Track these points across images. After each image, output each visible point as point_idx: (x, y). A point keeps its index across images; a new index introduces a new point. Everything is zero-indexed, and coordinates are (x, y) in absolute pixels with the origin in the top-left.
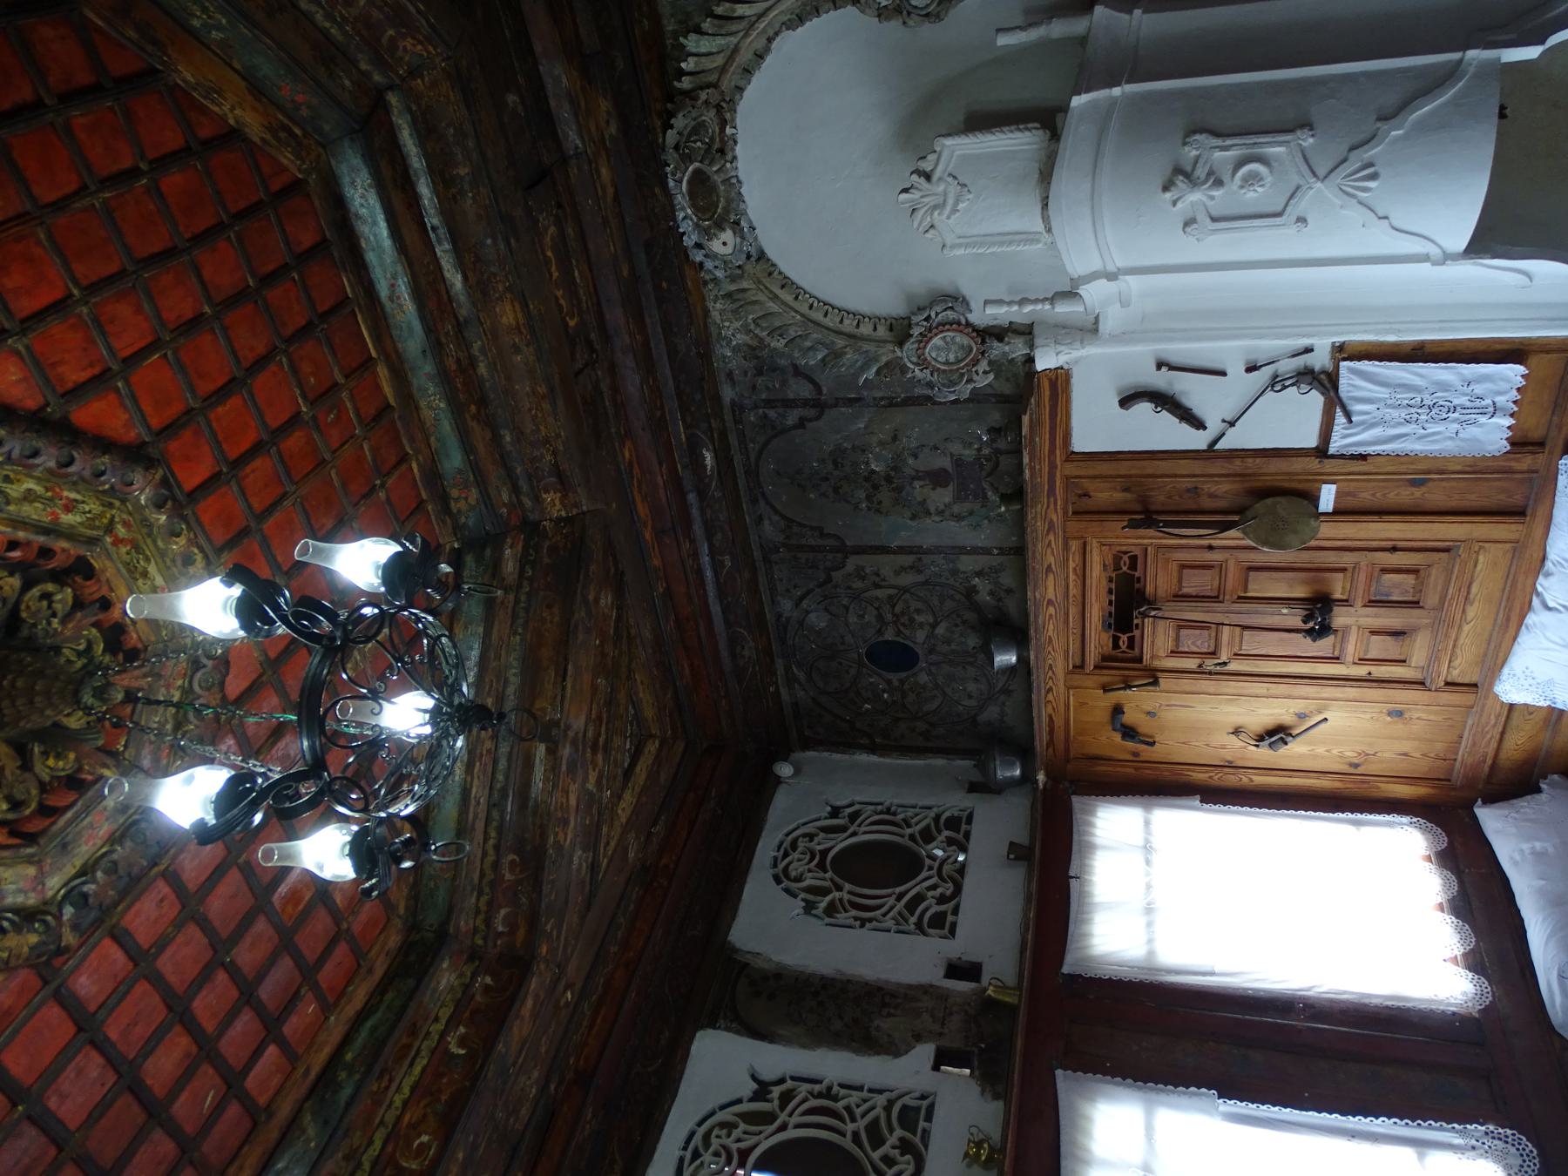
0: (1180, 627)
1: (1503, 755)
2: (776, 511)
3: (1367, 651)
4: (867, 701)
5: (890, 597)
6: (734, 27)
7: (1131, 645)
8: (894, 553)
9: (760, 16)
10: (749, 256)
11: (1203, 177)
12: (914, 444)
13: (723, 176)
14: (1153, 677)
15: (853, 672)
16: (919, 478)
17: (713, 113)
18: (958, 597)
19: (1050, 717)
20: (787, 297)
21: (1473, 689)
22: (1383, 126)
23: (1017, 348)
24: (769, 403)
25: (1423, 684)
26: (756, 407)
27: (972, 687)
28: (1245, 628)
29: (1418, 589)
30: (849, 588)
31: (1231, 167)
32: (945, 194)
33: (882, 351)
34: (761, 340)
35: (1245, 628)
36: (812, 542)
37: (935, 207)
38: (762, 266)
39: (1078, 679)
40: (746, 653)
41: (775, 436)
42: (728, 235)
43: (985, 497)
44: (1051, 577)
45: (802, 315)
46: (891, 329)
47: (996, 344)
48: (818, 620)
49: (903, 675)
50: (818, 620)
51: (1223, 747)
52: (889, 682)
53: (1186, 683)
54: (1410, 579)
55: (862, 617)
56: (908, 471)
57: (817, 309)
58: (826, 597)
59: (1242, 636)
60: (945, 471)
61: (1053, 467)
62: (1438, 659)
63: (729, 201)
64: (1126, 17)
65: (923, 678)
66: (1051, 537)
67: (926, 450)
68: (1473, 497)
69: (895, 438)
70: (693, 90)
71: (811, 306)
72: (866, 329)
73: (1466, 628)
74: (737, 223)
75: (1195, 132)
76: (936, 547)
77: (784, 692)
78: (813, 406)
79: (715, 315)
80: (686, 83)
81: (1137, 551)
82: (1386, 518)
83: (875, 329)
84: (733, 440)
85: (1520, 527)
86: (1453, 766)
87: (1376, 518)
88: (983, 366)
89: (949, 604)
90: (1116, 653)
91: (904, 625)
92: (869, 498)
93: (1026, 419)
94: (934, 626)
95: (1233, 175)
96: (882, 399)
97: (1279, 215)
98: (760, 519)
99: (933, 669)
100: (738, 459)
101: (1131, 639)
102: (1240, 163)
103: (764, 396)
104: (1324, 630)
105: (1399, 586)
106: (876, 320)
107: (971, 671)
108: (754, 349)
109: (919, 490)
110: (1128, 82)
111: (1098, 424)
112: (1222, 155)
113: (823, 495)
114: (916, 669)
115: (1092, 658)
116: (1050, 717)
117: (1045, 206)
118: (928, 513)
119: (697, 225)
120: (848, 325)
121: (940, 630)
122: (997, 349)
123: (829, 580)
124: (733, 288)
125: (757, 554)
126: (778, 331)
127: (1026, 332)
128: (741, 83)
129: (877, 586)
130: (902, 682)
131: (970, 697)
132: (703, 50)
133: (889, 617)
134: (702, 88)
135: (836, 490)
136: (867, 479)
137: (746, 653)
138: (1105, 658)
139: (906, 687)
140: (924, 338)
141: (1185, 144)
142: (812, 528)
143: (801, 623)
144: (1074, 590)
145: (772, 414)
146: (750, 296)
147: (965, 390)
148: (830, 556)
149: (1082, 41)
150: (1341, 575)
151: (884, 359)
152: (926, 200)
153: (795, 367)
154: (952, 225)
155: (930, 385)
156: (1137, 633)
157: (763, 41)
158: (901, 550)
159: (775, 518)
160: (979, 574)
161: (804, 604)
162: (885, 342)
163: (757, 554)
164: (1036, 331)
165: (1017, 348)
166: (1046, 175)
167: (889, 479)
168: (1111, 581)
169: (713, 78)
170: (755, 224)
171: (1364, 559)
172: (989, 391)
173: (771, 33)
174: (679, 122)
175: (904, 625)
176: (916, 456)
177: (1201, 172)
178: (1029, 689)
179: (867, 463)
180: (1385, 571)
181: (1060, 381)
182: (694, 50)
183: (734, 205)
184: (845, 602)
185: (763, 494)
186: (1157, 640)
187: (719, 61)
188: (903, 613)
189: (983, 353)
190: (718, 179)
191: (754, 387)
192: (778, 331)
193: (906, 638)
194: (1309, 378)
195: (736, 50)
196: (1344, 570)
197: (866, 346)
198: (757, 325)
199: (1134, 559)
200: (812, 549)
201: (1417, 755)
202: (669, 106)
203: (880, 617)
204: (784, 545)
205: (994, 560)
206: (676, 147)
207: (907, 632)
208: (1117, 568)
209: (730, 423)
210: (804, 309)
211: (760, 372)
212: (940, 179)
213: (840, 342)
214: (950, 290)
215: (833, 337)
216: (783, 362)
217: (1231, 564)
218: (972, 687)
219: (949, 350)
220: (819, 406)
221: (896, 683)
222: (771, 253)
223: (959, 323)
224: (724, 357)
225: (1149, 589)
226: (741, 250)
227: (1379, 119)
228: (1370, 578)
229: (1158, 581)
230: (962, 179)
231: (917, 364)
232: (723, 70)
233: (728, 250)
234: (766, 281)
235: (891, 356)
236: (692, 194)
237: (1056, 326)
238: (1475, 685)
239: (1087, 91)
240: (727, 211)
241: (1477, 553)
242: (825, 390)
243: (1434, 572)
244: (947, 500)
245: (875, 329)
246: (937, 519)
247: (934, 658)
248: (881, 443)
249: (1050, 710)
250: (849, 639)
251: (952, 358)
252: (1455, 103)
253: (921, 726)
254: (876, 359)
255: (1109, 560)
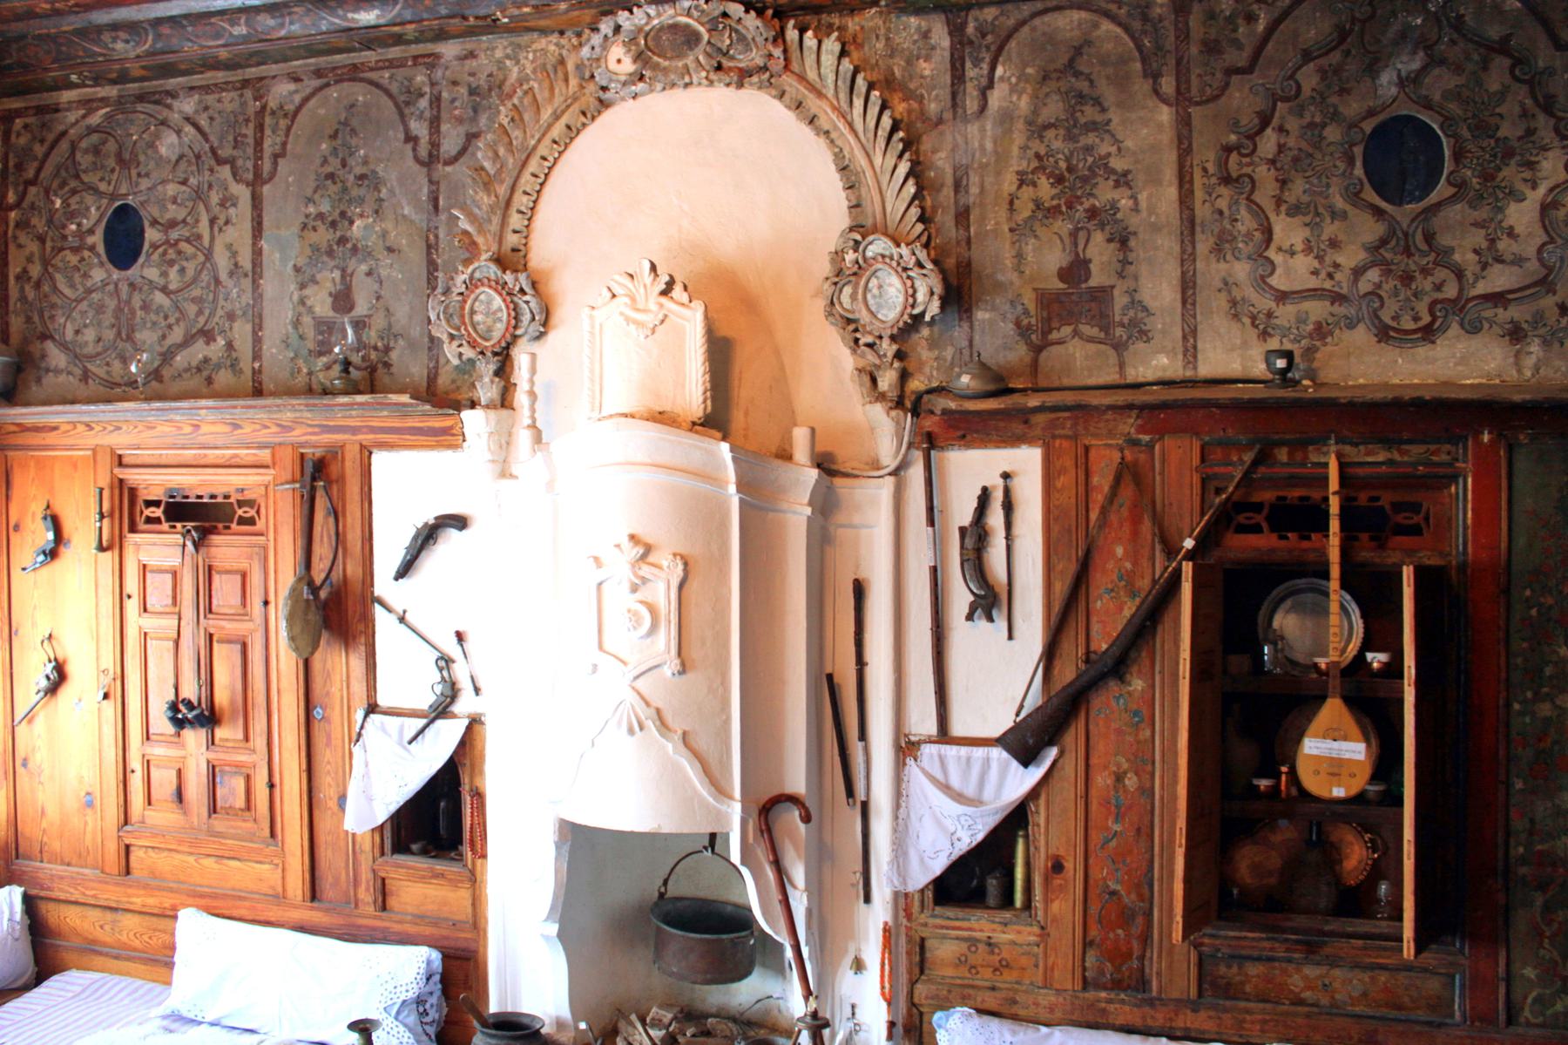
0: (175, 574)
1: (51, 906)
2: (306, 100)
3: (158, 766)
4: (66, 203)
5: (199, 237)
6: (843, 96)
7: (149, 520)
8: (254, 244)
9: (851, 125)
10: (604, 89)
11: (641, 573)
12: (384, 273)
13: (692, 66)
14: (110, 545)
15: (103, 187)
16: (343, 277)
17: (760, 62)
18: (202, 320)
19: (55, 428)
20: (557, 130)
21: (123, 870)
22: (677, 737)
23: (487, 390)
24: (436, 101)
25: (126, 823)
26: (433, 84)
27: (89, 335)
28: (177, 643)
29: (230, 811)
30: (210, 186)
31: (649, 600)
32: (645, 311)
33: (490, 238)
34: (510, 96)
35: (177, 643)
36: (267, 143)
37: (633, 299)
38: (593, 103)
39: (105, 461)
40: (120, 46)
41: (397, 105)
42: (628, 66)
43: (321, 354)
44: (227, 429)
45: (535, 148)
46: (515, 250)
47: (492, 367)
48: (168, 145)
49: (101, 249)
50: (168, 145)
51: (34, 624)
52: (91, 231)
53: (108, 581)
54: (240, 802)
55: (174, 201)
56: (352, 264)
57: (541, 165)
58: (198, 157)
59: (168, 639)
60: (351, 308)
61: (354, 430)
62: (155, 835)
63: (665, 71)
64: (806, 500)
65: (98, 275)
66: (274, 429)
67: (376, 286)
68: (329, 853)
69: (390, 250)
70: (784, 41)
71: (544, 159)
72: (516, 221)
73: (191, 859)
74: (642, 78)
75: (686, 564)
76: (261, 296)
77: (67, 96)
78: (430, 155)
79: (542, 43)
80: (792, 34)
81: (260, 525)
82: (304, 775)
83: (515, 232)
84: (395, 52)
85: (300, 898)
86: (29, 858)
87: (304, 766)
88: (468, 353)
89: (192, 309)
90: (140, 504)
91: (165, 253)
92: (321, 216)
93: (405, 398)
94: (164, 290)
95: (641, 602)
96: (437, 237)
97: (601, 648)
98: (297, 80)
99: (111, 287)
100: (369, 56)
101: (157, 521)
102: (653, 610)
103: (445, 95)
104: (180, 723)
105: (232, 790)
106: (526, 232)
107: (109, 335)
108: (500, 87)
109: (330, 278)
110: (741, 500)
111: (404, 485)
112: (662, 592)
113: (325, 161)
114: (110, 266)
115: (133, 476)
116: (55, 428)
117: (626, 416)
118: (302, 286)
119: (640, 30)
120: (521, 201)
121: (159, 298)
122: (487, 368)
123: (221, 162)
124: (570, 66)
125: (252, 72)
126: (517, 118)
127: (505, 401)
128: (787, 97)
129: (212, 222)
130: (92, 248)
131: (77, 332)
132: (823, 58)
133: (174, 235)
134: (785, 51)
135: (331, 176)
136: (343, 214)
137: (120, 46)
138: (133, 492)
139: (86, 254)
140: (500, 287)
141: (675, 555)
142: (284, 144)
143: (163, 123)
144: (213, 455)
145: (423, 103)
146: (559, 87)
147: (441, 331)
148: (250, 164)
149: (786, 455)
150: (240, 736)
151: (480, 240)
152: (642, 290)
153: (476, 136)
154: (612, 315)
155: (447, 291)
156: (165, 526)
157: (826, 127)
158: (257, 253)
159: (297, 99)
160: (230, 346)
161: (189, 129)
162: (500, 243)
163: (252, 72)
164: (505, 413)
165: (487, 390)
166: (661, 418)
167: (342, 241)
168: (226, 497)
169: (795, 66)
170: (640, 100)
171: (260, 759)
172: (442, 361)
173: (834, 135)
174: (751, 21)
175: (165, 253)
176: (369, 274)
177: (645, 570)
178: (89, 401)
179: (361, 216)
180: (248, 778)
181: (449, 438)
182: (824, 47)
183: (660, 76)
184: (193, 181)
185: (328, 85)
186: (161, 549)
187: (812, 75)
188: (179, 253)
189: (482, 353)
190: (690, 60)
191: (455, 83)
192: (517, 118)
193: (149, 255)
194: (449, 693)
195: (820, 94)
196: (247, 739)
197: (496, 220)
198: (526, 93)
199: (251, 521)
200: (259, 143)
201: (44, 825)
202: (770, 12)
203: (173, 224)
204: (264, 108)
205: (246, 365)
206: (725, 15)
207: (156, 257)
208: (241, 504)
209: (416, 49)
210: (543, 150)
211: (473, 92)
212: (661, 306)
213: (502, 190)
214: (554, 320)
215: (509, 182)
216: (483, 120)
217: (250, 625)
218: (89, 335)
219: (487, 315)
220: (430, 161)
221: (90, 240)
222: (607, 116)
223: (515, 327)
224: (493, 49)
225: (216, 539)
226: (611, 80)
227: (685, 733)
228: (239, 765)
229: (227, 548)
230: (660, 329)
231: (471, 278)
232: (802, 78)
233: (612, 65)
234: (576, 108)
235: (483, 247)
236: (675, 27)
237: (510, 434)
238: (128, 873)
239: (735, 459)
240: (656, 67)
241: (271, 863)
242: (448, 169)
243: (250, 825)
244: (318, 310)
245: (515, 232)
246: (296, 297)
247: (124, 288)
248: (384, 234)
249: (64, 428)
250: (145, 184)
251: (478, 318)
252: (702, 800)
253: (35, 270)
254: (481, 231)
255: (248, 495)
